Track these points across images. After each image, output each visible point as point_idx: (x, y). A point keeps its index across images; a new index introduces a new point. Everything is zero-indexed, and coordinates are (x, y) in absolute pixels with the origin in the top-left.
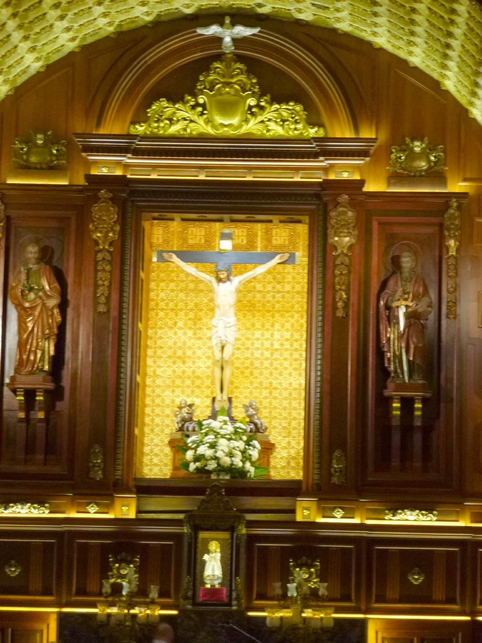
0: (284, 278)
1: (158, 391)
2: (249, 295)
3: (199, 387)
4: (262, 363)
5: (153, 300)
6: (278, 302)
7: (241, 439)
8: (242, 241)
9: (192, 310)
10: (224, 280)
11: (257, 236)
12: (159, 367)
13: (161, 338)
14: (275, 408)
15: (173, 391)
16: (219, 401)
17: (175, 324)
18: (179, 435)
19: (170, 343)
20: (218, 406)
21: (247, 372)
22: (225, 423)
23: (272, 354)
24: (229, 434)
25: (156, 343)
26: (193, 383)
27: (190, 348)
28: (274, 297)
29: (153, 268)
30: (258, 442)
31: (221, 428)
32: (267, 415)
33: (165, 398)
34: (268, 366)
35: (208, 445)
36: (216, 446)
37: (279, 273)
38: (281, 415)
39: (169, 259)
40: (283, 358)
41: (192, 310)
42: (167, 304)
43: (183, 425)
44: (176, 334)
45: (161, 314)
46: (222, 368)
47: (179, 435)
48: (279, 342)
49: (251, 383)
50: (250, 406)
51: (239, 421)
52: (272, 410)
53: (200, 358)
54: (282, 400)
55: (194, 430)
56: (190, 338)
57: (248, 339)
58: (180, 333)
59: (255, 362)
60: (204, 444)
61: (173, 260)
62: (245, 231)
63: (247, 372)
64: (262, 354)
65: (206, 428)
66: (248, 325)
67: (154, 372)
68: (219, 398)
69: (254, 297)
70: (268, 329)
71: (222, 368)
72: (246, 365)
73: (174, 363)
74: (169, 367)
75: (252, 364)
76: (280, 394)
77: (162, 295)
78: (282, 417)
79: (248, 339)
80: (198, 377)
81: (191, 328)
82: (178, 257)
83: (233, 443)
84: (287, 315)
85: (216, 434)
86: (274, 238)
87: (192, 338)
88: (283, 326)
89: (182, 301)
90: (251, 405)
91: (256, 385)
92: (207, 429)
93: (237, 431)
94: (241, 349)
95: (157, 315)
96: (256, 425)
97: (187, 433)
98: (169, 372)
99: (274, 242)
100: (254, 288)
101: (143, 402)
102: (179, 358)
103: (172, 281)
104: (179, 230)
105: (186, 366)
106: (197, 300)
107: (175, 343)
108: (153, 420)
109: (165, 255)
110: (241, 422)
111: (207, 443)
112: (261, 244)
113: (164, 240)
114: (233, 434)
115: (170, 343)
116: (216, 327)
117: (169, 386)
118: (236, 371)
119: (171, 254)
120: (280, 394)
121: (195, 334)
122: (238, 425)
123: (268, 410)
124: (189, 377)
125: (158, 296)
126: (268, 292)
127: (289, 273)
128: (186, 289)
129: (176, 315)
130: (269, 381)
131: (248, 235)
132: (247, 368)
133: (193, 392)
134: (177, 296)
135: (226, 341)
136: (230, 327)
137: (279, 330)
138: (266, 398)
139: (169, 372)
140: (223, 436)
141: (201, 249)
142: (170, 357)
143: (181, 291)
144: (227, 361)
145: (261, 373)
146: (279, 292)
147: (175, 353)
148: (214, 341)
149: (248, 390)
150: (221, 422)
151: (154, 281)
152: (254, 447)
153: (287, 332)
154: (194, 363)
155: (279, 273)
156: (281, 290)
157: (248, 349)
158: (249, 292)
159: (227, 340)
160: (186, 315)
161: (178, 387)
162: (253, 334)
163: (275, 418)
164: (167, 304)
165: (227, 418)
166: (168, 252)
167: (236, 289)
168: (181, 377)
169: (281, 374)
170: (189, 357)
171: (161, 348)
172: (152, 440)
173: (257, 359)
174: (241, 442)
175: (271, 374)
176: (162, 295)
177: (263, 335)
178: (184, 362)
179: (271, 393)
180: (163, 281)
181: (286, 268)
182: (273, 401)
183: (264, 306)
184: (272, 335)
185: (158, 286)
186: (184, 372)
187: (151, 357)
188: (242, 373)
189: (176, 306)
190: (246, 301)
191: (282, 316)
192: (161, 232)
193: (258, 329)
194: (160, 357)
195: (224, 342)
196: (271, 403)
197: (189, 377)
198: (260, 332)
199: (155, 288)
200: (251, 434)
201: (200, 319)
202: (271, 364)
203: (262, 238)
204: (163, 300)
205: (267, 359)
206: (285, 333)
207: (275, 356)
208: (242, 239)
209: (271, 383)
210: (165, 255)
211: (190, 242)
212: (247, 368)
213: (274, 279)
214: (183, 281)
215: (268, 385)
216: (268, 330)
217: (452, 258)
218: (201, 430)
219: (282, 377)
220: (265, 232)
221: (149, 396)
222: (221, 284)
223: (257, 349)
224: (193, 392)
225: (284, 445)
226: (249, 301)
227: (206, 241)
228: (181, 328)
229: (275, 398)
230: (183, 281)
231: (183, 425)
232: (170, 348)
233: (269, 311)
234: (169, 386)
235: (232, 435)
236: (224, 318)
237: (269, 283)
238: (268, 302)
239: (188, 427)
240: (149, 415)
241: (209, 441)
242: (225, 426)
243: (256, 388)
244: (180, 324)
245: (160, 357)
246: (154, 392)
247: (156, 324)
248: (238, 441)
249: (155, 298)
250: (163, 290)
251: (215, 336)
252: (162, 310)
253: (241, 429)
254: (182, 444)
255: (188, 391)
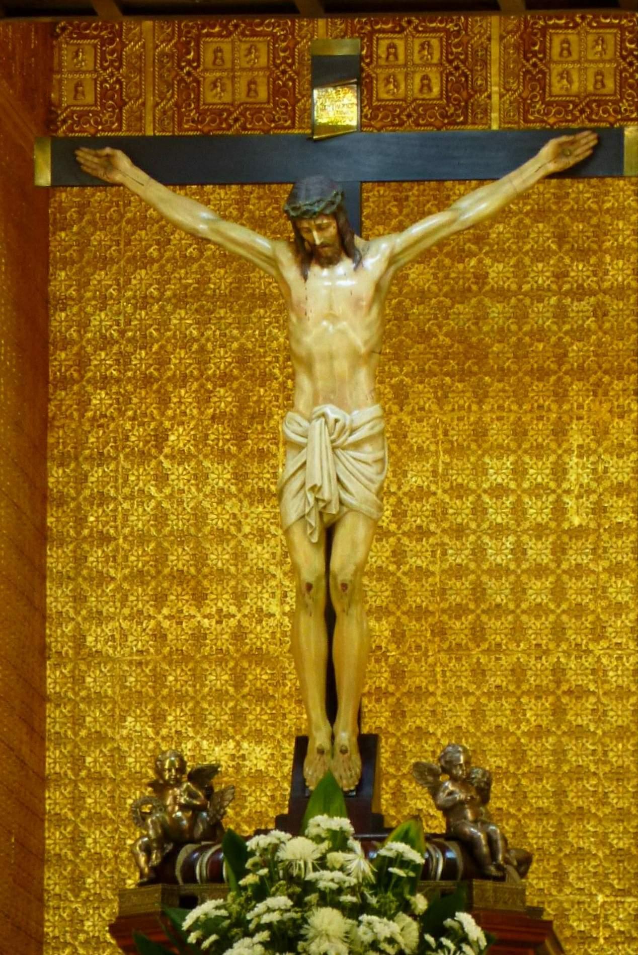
0: (600, 232)
1: (94, 718)
2: (459, 307)
3: (262, 697)
4: (518, 591)
5: (66, 344)
6: (581, 334)
7: (406, 907)
8: (426, 84)
9: (225, 379)
10: (328, 251)
11: (485, 63)
12: (99, 617)
13: (103, 499)
14: (579, 773)
15: (158, 719)
16: (321, 752)
17: (160, 438)
18: (152, 900)
19: (139, 519)
20: (313, 773)
21: (460, 627)
22: (339, 841)
23: (559, 551)
24: (353, 890)
25: (81, 522)
26: (238, 683)
27: (222, 536)
28: (561, 314)
29: (61, 210)
30: (474, 916)
31: (322, 863)
32: (544, 803)
33: (124, 746)
34: (544, 599)
35: (264, 935)
36: (303, 938)
37: (581, 214)
38: (603, 801)
39: (100, 173)
40: (606, 564)
41: (225, 379)
42: (123, 360)
43: (169, 859)
44: (162, 479)
45: (100, 399)
46: (330, 618)
47: (152, 900)
48: (587, 503)
49: (479, 672)
50: (445, 771)
51: (394, 834)
52: (565, 782)
53: (263, 576)
54: (607, 740)
55: (215, 876)
56: (222, 496)
57: (459, 491)
58: (179, 474)
59: (491, 584)
60: (251, 935)
61: (118, 178)
62: (435, 43)
63: (460, 627)
64: (519, 552)
65: (256, 866)
66: (459, 432)
67: (79, 640)
68: (320, 739)
69: (480, 318)
70: (540, 446)
71: (330, 618)
72: (454, 599)
73: (160, 600)
74: (138, 616)
75: (479, 592)
76: (599, 715)
77: (101, 320)
78: (607, 810)
79: (459, 491)
80: (259, 657)
81: (223, 456)
82: (137, 162)
83: (369, 924)
84: (618, 385)
85: (298, 890)
86: (556, 69)
87: (230, 495)
88: (601, 432)
89: (185, 343)
90: (448, 767)
91: (494, 681)
92: (264, 871)
93: (391, 875)
94: (431, 534)
95: (84, 404)
96: (468, 845)
97: (191, 888)
98: (139, 639)
99: (557, 86)
100: (481, 278)
101: (379, 760)
102: (180, 577)
103: (146, 262)
104: (167, 48)
105: (207, 611)
106: (249, 339)
107: (160, 517)
108: (77, 840)
109: (85, 156)
110: (405, 838)
111: (260, 928)
112: (501, 96)
113: (104, 95)
114: (372, 887)
115: (139, 519)
116: (300, 447)
117: (140, 698)
118: (414, 625)
119: (108, 150)
120: (599, 715)
121: (240, 477)
122: (394, 847)
123: (548, 785)
124: (222, 658)
125: (84, 326)
126: (538, 295)
127: (620, 213)
128: (199, 294)
129: (164, 401)
130: (547, 662)
131: (448, 58)
132: (459, 611)
133: (238, 717)
134: (163, 325)
135: (341, 503)
136: (357, 445)
137: (583, 451)
138: (539, 733)
139: (139, 639)
140: (329, 899)
141: (255, 130)
142: (139, 577)
143: (180, 301)
144: (344, 586)
145: (517, 632)
146: (580, 293)
147: (160, 558)
148: (293, 508)
149: (467, 704)
150: (318, 839)
151: (66, 263)
152: (461, 938)
153: (620, 456)
154: (239, 597)
155: (581, 214)
156: (591, 283)
157: (459, 532)
158: (464, 294)
159: (345, 496)
160: (204, 399)
161: (179, 699)
162: (480, 470)
163: (581, 814)
164: (123, 360)
165: (343, 823)
166: (95, 143)
167: (378, 288)
168: (186, 658)
169: (598, 633)
170: (221, 575)
171: (105, 539)
172: (76, 921)
173: (499, 571)
174: (406, 919)
175: (559, 632)
176: (101, 320)
177: (519, 472)
178: (199, 598)
179: (559, 711)
180: (105, 262)
181: (607, 193)
182: (571, 745)
183: (520, 353)
184: (559, 472)
185: (83, 285)
186: (199, 636)
187: (63, 579)
188: (440, 632)
189: (162, 362)
190: (446, 335)
191: (598, 390)
192: (87, 60)
193: (500, 446)
194: (102, 579)
195: (334, 509)
196: (559, 754)
197: (222, 658)
198: (509, 462)
199: (72, 292)
200: (448, 884)
201: (261, 416)
202: (559, 592)
203: (505, 71)
204: (106, 342)
205: (540, 571)
206: (612, 461)
207: (573, 558)
208: (425, 77)
209: (558, 672)
210: (85, 156)
211: (210, 97)
212: (459, 611)
213: (561, 238)
214: (188, 261)
215: (546, 681)
216: (539, 451)
217: (119, 219)
218: (241, 873)
219: (604, 644)
220: (517, 47)
221: (60, 740)
222: (315, 270)
223: (499, 531)
224: (238, 717)
225: (616, 926)
226: (460, 336)
227: (277, 91)
228: (181, 457)
229: (579, 732)
230: (188, 261)
231: (169, 859)
232: (142, 539)
233: (542, 374)
234: (140, 698)
235: (367, 892)
236: (332, 412)
237: (541, 255)
238: (540, 334)
239: (189, 867)
240: (60, 821)
241: (266, 919)
242: (337, 857)
243: (500, 692)
244: (178, 438)
245: (102, 579)
246: (77, 721)
247: (80, 444)
248: (391, 918)
249: (73, 333)
250: (103, 302)
251: (296, 484)
252: (105, 382)
253: (404, 863)
254: (165, 937)
255: (218, 716)
